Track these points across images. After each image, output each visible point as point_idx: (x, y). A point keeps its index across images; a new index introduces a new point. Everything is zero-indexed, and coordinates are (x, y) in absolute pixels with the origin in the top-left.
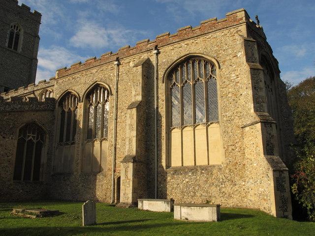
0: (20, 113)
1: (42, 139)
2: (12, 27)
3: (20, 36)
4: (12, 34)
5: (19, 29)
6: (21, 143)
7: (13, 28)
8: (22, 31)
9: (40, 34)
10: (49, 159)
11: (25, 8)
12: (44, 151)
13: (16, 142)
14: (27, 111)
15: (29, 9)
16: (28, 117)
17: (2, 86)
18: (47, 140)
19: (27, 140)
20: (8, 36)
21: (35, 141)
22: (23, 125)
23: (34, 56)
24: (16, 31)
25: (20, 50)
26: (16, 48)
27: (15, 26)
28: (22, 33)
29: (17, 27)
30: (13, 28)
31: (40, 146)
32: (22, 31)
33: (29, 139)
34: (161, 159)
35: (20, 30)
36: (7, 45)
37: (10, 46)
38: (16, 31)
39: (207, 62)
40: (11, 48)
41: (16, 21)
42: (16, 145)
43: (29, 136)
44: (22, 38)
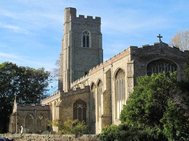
0: (72, 96)
1: (86, 106)
2: (83, 33)
3: (89, 38)
4: (84, 37)
5: (88, 33)
6: (75, 110)
7: (84, 34)
8: (90, 33)
9: (102, 31)
10: (90, 116)
11: (90, 18)
12: (87, 111)
13: (72, 110)
14: (76, 94)
15: (92, 17)
16: (76, 98)
17: (83, 72)
18: (88, 107)
19: (78, 108)
20: (82, 40)
21: (82, 108)
22: (75, 101)
23: (100, 48)
24: (86, 35)
25: (90, 46)
26: (88, 46)
27: (85, 32)
28: (90, 35)
29: (87, 32)
30: (84, 34)
31: (85, 110)
32: (90, 33)
33: (79, 107)
34: (95, 106)
35: (88, 34)
36: (82, 46)
37: (84, 46)
38: (86, 35)
39: (83, 102)
40: (85, 46)
41: (85, 29)
42: (72, 110)
43: (79, 106)
44: (90, 38)
